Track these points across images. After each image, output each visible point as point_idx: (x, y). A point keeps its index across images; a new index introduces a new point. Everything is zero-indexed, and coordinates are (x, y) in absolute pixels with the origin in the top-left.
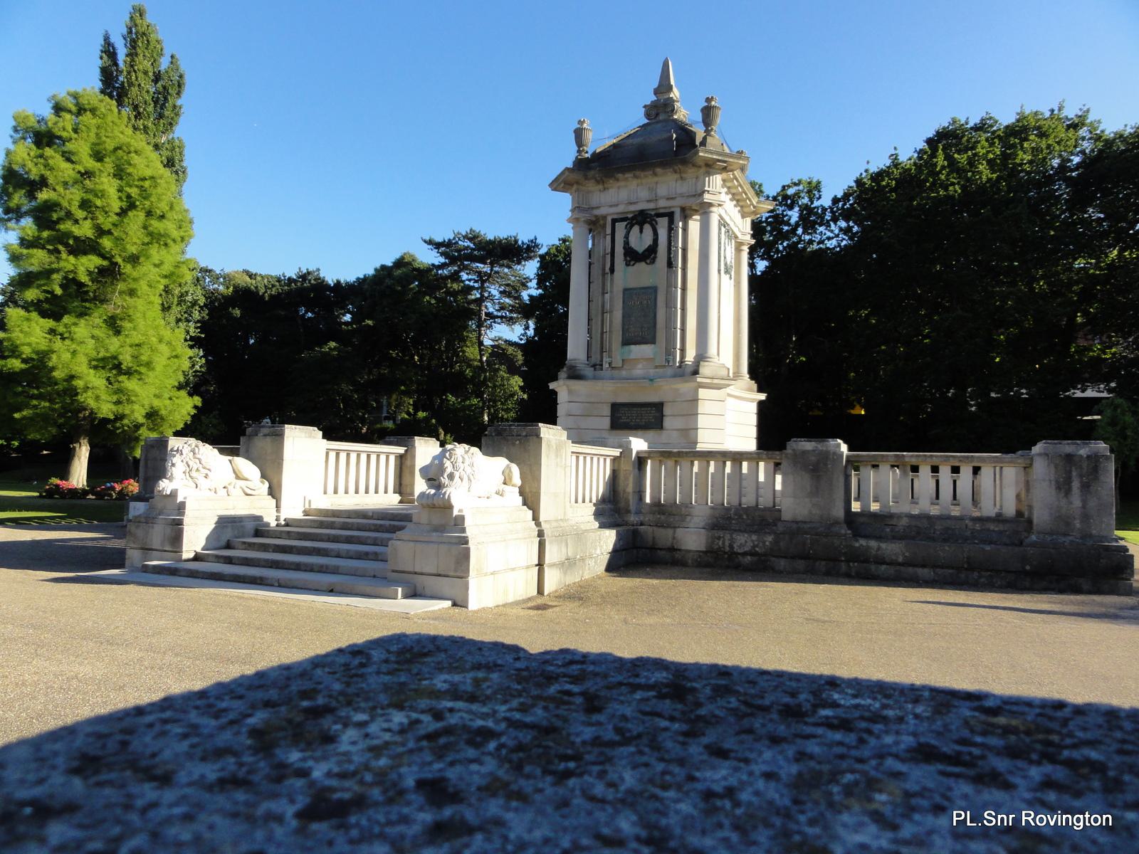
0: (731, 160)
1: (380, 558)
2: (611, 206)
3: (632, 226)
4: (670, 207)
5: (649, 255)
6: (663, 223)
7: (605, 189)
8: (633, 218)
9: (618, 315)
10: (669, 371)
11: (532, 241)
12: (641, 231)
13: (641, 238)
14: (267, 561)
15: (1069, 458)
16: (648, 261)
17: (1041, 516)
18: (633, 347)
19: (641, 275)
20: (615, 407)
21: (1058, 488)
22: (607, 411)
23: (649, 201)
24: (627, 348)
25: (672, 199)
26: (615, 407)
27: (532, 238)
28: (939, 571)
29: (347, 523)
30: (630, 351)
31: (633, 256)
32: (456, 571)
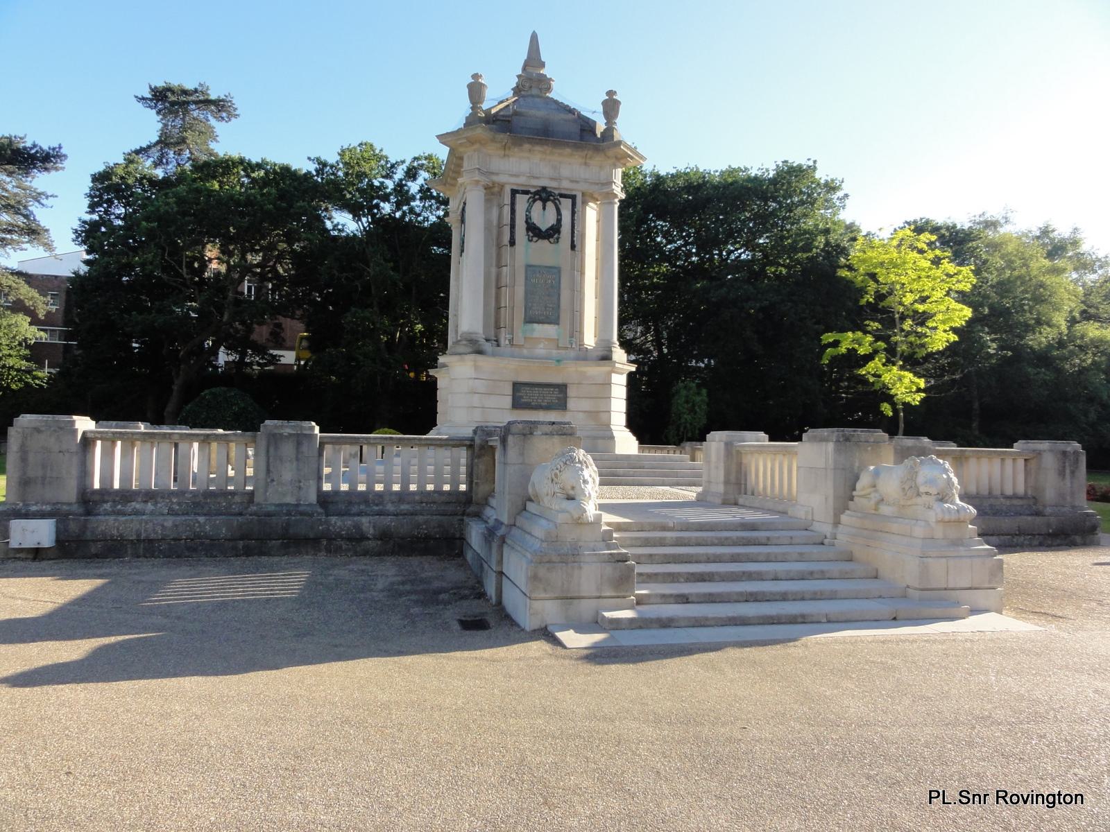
0: (637, 158)
1: (828, 576)
2: (512, 175)
3: (534, 201)
4: (572, 190)
5: (552, 233)
6: (566, 205)
7: (505, 155)
8: (536, 193)
9: (520, 291)
10: (572, 354)
11: (54, 149)
12: (544, 208)
13: (544, 214)
14: (741, 594)
15: (1064, 453)
16: (551, 240)
17: (1050, 495)
18: (535, 325)
19: (543, 252)
20: (517, 386)
21: (1060, 474)
22: (508, 390)
23: (552, 179)
24: (529, 326)
25: (577, 182)
26: (517, 386)
27: (56, 145)
28: (1002, 538)
29: (681, 538)
30: (533, 330)
31: (534, 231)
32: (990, 582)
